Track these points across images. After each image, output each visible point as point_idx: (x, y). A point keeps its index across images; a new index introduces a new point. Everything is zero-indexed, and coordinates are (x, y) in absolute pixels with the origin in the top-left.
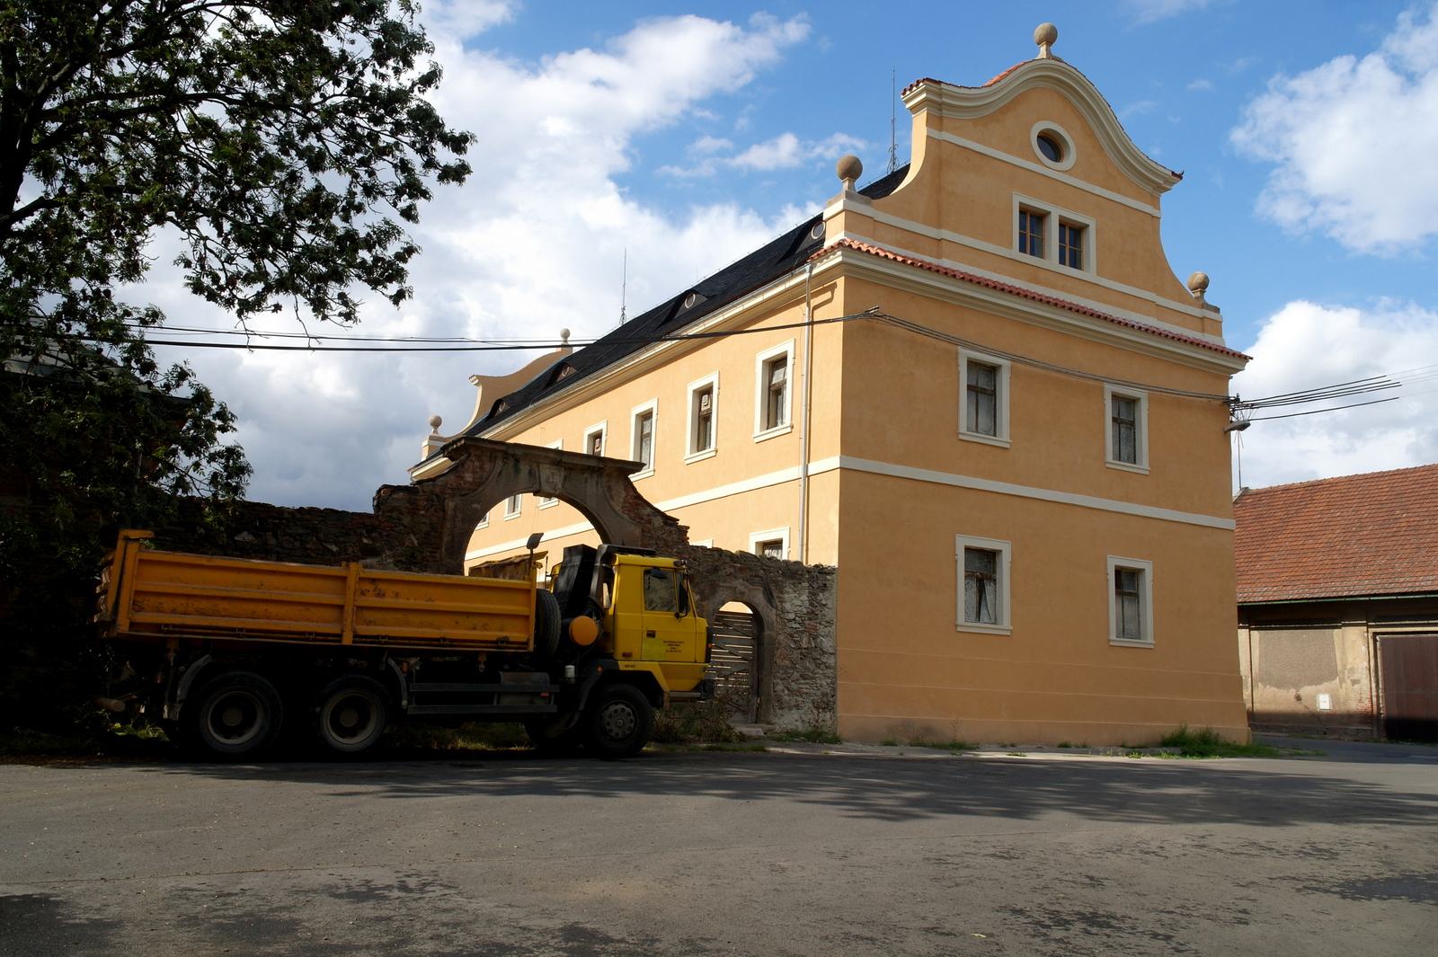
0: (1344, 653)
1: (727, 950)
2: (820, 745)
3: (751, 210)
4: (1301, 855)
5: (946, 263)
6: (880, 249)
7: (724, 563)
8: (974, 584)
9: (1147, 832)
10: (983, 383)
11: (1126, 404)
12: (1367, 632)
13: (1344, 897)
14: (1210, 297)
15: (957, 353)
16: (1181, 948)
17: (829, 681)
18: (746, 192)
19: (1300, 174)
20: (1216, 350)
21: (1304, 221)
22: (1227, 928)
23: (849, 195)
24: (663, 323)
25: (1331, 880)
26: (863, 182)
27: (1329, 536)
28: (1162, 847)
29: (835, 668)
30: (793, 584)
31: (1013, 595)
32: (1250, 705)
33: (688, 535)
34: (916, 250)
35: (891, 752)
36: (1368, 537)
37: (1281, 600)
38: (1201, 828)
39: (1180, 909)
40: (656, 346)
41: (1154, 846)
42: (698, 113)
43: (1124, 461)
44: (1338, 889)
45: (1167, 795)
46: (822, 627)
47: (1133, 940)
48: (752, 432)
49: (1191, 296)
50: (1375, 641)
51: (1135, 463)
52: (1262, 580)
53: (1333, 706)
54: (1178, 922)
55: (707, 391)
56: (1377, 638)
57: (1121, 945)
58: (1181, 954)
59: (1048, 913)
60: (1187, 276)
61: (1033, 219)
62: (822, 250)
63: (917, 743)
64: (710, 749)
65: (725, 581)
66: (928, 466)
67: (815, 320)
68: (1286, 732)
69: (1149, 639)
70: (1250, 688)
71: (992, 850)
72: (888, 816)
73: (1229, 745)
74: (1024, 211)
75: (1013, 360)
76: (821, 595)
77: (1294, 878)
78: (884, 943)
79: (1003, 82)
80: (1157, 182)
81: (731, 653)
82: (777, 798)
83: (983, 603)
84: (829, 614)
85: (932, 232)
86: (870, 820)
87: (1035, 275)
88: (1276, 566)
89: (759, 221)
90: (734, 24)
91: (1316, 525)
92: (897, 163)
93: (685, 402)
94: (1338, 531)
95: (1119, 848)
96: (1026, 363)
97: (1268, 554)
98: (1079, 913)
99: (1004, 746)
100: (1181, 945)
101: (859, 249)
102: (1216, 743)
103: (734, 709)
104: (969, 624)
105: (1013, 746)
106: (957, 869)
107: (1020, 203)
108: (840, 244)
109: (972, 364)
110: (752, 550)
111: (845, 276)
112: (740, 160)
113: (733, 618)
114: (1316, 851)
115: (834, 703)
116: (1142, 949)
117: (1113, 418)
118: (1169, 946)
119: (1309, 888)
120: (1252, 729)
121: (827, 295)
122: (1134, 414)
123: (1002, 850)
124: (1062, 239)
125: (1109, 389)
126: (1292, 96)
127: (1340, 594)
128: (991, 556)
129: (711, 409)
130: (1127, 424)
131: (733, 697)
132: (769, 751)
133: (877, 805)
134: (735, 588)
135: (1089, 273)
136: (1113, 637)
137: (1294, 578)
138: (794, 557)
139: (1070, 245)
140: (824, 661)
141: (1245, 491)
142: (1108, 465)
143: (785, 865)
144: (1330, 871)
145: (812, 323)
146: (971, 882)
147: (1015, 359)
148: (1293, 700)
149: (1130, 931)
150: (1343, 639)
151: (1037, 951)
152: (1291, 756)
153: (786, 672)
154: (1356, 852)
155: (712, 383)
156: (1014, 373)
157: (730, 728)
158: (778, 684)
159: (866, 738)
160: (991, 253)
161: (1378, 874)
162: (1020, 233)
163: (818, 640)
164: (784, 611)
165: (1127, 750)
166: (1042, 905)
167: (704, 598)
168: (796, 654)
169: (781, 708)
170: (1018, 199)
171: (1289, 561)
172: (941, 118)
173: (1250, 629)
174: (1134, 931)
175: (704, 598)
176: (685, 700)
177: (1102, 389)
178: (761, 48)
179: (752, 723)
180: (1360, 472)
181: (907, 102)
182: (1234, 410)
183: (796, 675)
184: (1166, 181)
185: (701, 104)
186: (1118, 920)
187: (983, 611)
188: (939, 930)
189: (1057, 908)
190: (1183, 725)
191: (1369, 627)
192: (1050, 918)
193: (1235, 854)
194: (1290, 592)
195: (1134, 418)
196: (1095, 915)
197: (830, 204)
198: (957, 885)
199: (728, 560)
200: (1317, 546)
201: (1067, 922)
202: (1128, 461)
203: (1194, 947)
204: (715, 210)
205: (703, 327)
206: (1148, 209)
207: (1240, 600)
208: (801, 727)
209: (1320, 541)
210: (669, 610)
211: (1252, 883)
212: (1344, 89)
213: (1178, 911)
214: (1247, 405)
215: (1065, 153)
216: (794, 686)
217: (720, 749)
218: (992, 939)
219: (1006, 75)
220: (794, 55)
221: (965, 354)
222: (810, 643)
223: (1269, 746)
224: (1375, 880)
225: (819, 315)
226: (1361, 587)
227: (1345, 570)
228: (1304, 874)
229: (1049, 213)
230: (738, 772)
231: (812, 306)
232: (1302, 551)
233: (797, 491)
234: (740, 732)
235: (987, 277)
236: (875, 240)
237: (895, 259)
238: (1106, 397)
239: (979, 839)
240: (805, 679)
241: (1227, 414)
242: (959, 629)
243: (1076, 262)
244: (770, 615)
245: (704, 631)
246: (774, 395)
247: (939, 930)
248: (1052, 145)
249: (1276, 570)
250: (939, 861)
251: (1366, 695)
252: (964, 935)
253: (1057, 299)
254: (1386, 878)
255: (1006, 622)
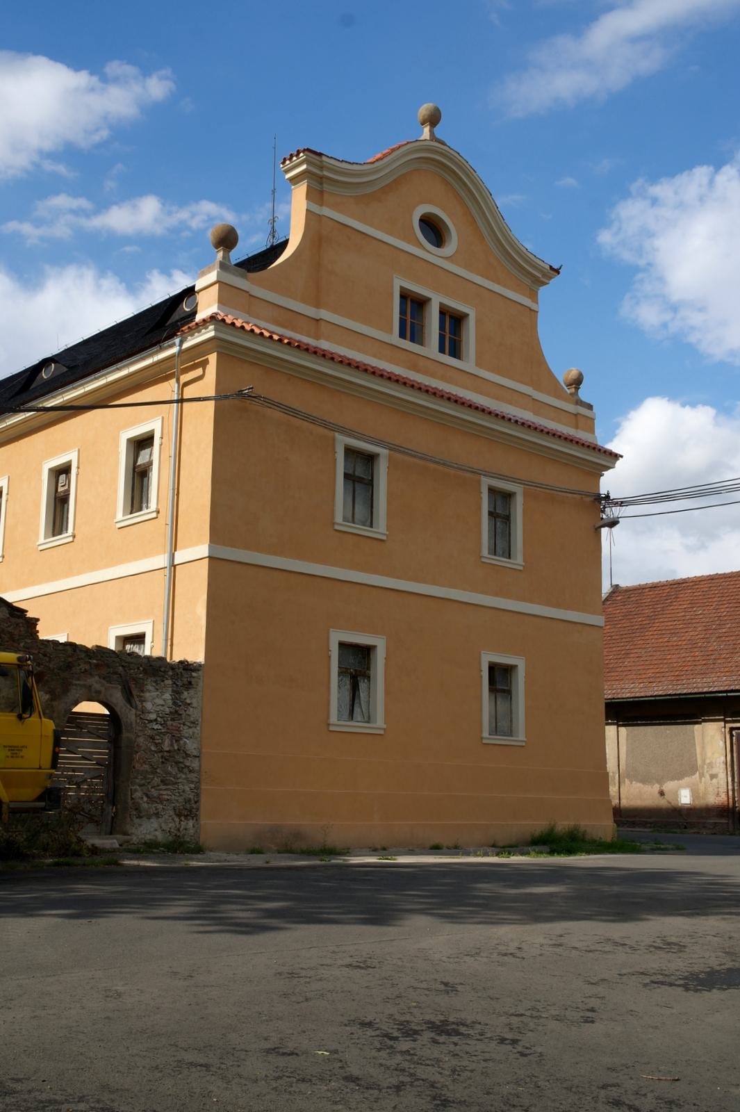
0: (703, 748)
1: (38, 1090)
2: (181, 856)
3: (110, 274)
4: (652, 949)
5: (325, 345)
6: (255, 325)
7: (79, 659)
8: (347, 681)
9: (508, 933)
10: (360, 471)
11: (502, 499)
12: (725, 727)
13: (687, 990)
14: (584, 394)
15: (334, 439)
16: (528, 1052)
17: (193, 786)
18: (112, 257)
19: (661, 280)
20: (589, 447)
21: (665, 326)
22: (573, 1028)
23: (224, 266)
24: (13, 397)
25: (678, 973)
26: (241, 252)
27: (691, 634)
28: (520, 948)
29: (199, 772)
30: (156, 682)
31: (387, 692)
32: (618, 801)
33: (38, 628)
34: (294, 329)
35: (257, 861)
36: (726, 634)
37: (646, 697)
38: (559, 927)
39: (530, 1012)
40: (8, 418)
41: (512, 948)
42: (48, 166)
43: (499, 556)
44: (682, 982)
45: (531, 894)
46: (186, 727)
47: (480, 1046)
48: (114, 516)
49: (566, 392)
50: (732, 736)
51: (510, 558)
52: (630, 677)
53: (693, 801)
54: (526, 1025)
55: (65, 470)
56: (734, 733)
57: (467, 1053)
58: (525, 1058)
59: (398, 1024)
60: (562, 371)
61: (414, 305)
62: (194, 323)
63: (287, 850)
64: (57, 864)
65: (79, 680)
66: (301, 556)
67: (185, 397)
68: (650, 827)
69: (521, 736)
70: (617, 784)
71: (348, 961)
72: (244, 929)
73: (596, 841)
74: (405, 296)
75: (391, 449)
76: (185, 693)
77: (642, 973)
78: (219, 1068)
79: (386, 160)
80: (536, 275)
81: (84, 758)
82: (124, 915)
83: (356, 701)
84: (194, 713)
85: (311, 311)
86: (223, 935)
87: (414, 362)
88: (642, 663)
89: (122, 287)
90: (92, 74)
91: (680, 622)
92: (276, 236)
93: (40, 480)
94: (700, 629)
95: (478, 951)
96: (403, 453)
97: (635, 651)
98: (430, 1022)
99: (375, 850)
100: (527, 1048)
101: (233, 324)
102: (583, 840)
103: (87, 820)
104: (340, 723)
105: (384, 849)
106: (309, 983)
107: (401, 287)
108: (213, 318)
109: (350, 452)
110: (112, 645)
111: (218, 352)
112: (97, 222)
113: (88, 719)
114: (668, 946)
115: (198, 809)
116: (487, 1056)
117: (489, 511)
118: (515, 1051)
119: (656, 983)
120: (618, 826)
121: (199, 372)
122: (509, 508)
123: (360, 960)
124: (442, 327)
125: (486, 482)
126: (655, 202)
127: (700, 690)
128: (363, 653)
129: (68, 490)
130: (503, 518)
131: (85, 806)
132: (122, 865)
133: (232, 918)
134: (90, 686)
135: (468, 364)
136: (486, 734)
137: (658, 675)
138: (158, 653)
139: (450, 333)
140: (188, 764)
141: (616, 589)
142: (483, 560)
143: (120, 989)
144: (678, 964)
145: (181, 401)
146: (322, 995)
147: (393, 448)
148: (657, 795)
149: (479, 1037)
150: (703, 734)
151: (381, 1065)
152: (653, 851)
153: (145, 778)
154: (702, 944)
155: (70, 461)
156: (392, 463)
157: (80, 841)
158: (136, 791)
159: (231, 846)
160: (371, 338)
161: (720, 965)
162: (400, 318)
163: (182, 742)
164: (144, 711)
165: (498, 850)
166: (392, 1015)
167: (54, 696)
168: (157, 758)
169: (139, 817)
170: (399, 283)
171: (655, 658)
172: (322, 192)
173: (619, 726)
174: (482, 1037)
175: (54, 696)
176: (27, 810)
177: (479, 482)
178: (123, 97)
179: (106, 834)
180: (721, 572)
181: (287, 171)
182: (605, 507)
183: (157, 780)
184: (544, 275)
185: (53, 156)
186: (467, 1026)
187: (357, 709)
188: (281, 1051)
189: (408, 1017)
190: (553, 823)
191: (726, 722)
192: (399, 1029)
193: (590, 951)
194: (656, 688)
195: (509, 512)
196: (445, 1023)
197: (203, 274)
198: (307, 1000)
199: (83, 655)
200: (680, 643)
201: (416, 1032)
202: (503, 556)
203: (539, 1050)
204: (71, 272)
205: (62, 400)
206: (526, 301)
207: (610, 697)
208: (160, 837)
209: (683, 638)
210: (11, 711)
211: (603, 980)
212: (701, 199)
213: (528, 1013)
214: (617, 503)
215: (447, 244)
216: (154, 793)
217: (68, 864)
218: (336, 1056)
219: (389, 154)
220: (153, 112)
221: (342, 441)
222: (172, 745)
223: (634, 841)
224: (717, 971)
225: (189, 392)
226: (720, 684)
227: (705, 667)
228: (653, 968)
229: (467, 315)
230: (85, 889)
231: (181, 383)
232: (667, 648)
233: (162, 580)
234: (93, 845)
235: (358, 360)
236: (250, 316)
237: (271, 337)
238: (482, 491)
239: (336, 949)
240: (166, 784)
241: (597, 511)
242: (332, 728)
243: (455, 352)
244: (129, 715)
245: (50, 733)
246: (139, 477)
247: (281, 1051)
248: (434, 230)
249: (642, 667)
250: (292, 975)
251: (723, 789)
252: (307, 1053)
253: (436, 388)
254: (728, 969)
255: (380, 721)
